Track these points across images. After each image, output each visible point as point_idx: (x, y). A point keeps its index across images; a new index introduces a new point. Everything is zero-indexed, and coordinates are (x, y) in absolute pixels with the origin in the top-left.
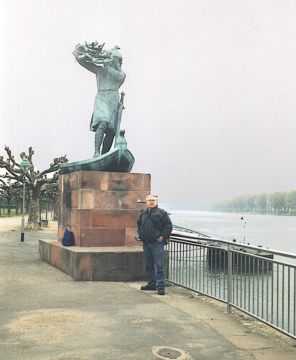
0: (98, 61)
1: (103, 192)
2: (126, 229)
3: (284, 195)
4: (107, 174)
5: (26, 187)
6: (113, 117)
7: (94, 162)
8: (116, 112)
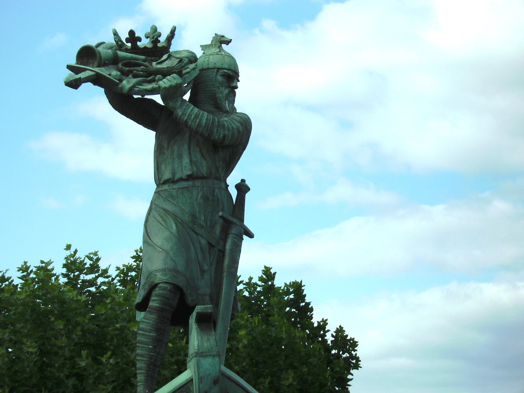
0: (138, 76)
6: (206, 267)
8: (220, 250)
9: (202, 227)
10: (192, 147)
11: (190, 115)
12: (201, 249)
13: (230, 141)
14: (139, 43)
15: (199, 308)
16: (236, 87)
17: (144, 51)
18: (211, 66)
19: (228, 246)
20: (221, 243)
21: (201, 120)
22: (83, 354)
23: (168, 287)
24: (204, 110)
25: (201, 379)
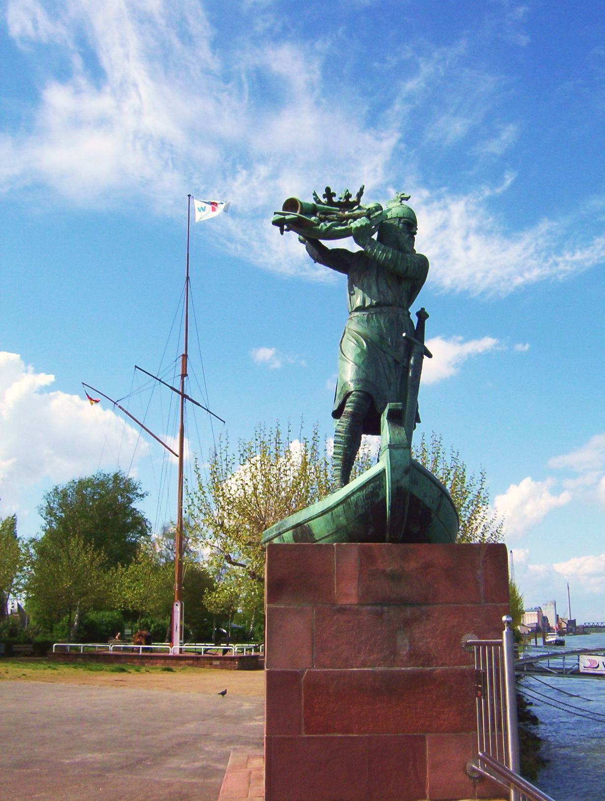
1: (342, 610)
3: (442, 339)
7: (318, 516)
9: (389, 346)
12: (389, 366)
13: (414, 273)
16: (415, 233)
17: (339, 204)
20: (405, 360)
22: (522, 37)
25: (393, 469)
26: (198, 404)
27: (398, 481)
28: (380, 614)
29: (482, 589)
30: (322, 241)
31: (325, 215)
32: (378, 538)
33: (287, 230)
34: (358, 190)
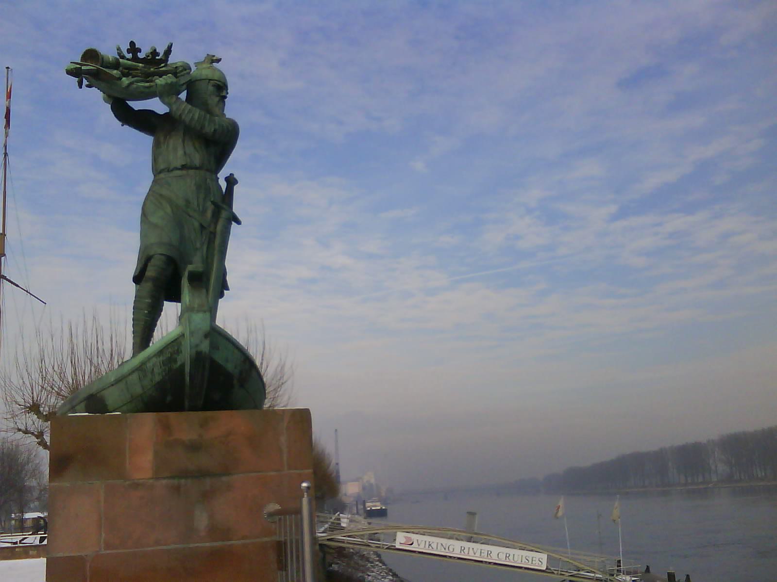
1: (136, 486)
2: (80, 60)
4: (149, 418)
5: (150, 55)
8: (211, 232)
10: (186, 142)
11: (184, 110)
13: (220, 142)
14: (139, 53)
15: (190, 268)
18: (203, 77)
19: (219, 228)
21: (193, 115)
23: (163, 257)
24: (196, 106)
25: (192, 333)
26: (17, 286)
27: (197, 346)
28: (177, 489)
29: (285, 458)
30: (130, 103)
31: (128, 71)
32: (177, 406)
33: (89, 86)
34: (166, 48)
